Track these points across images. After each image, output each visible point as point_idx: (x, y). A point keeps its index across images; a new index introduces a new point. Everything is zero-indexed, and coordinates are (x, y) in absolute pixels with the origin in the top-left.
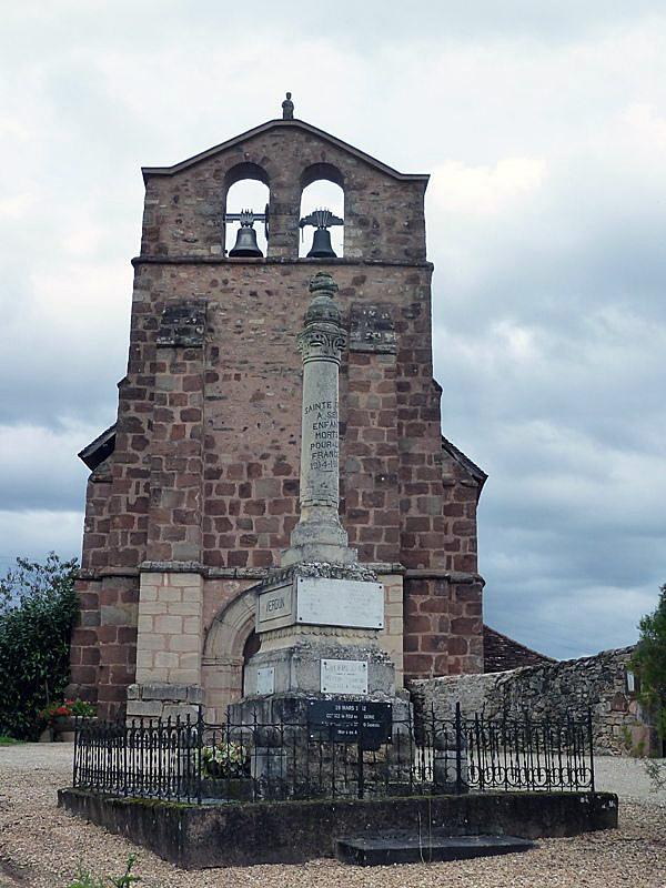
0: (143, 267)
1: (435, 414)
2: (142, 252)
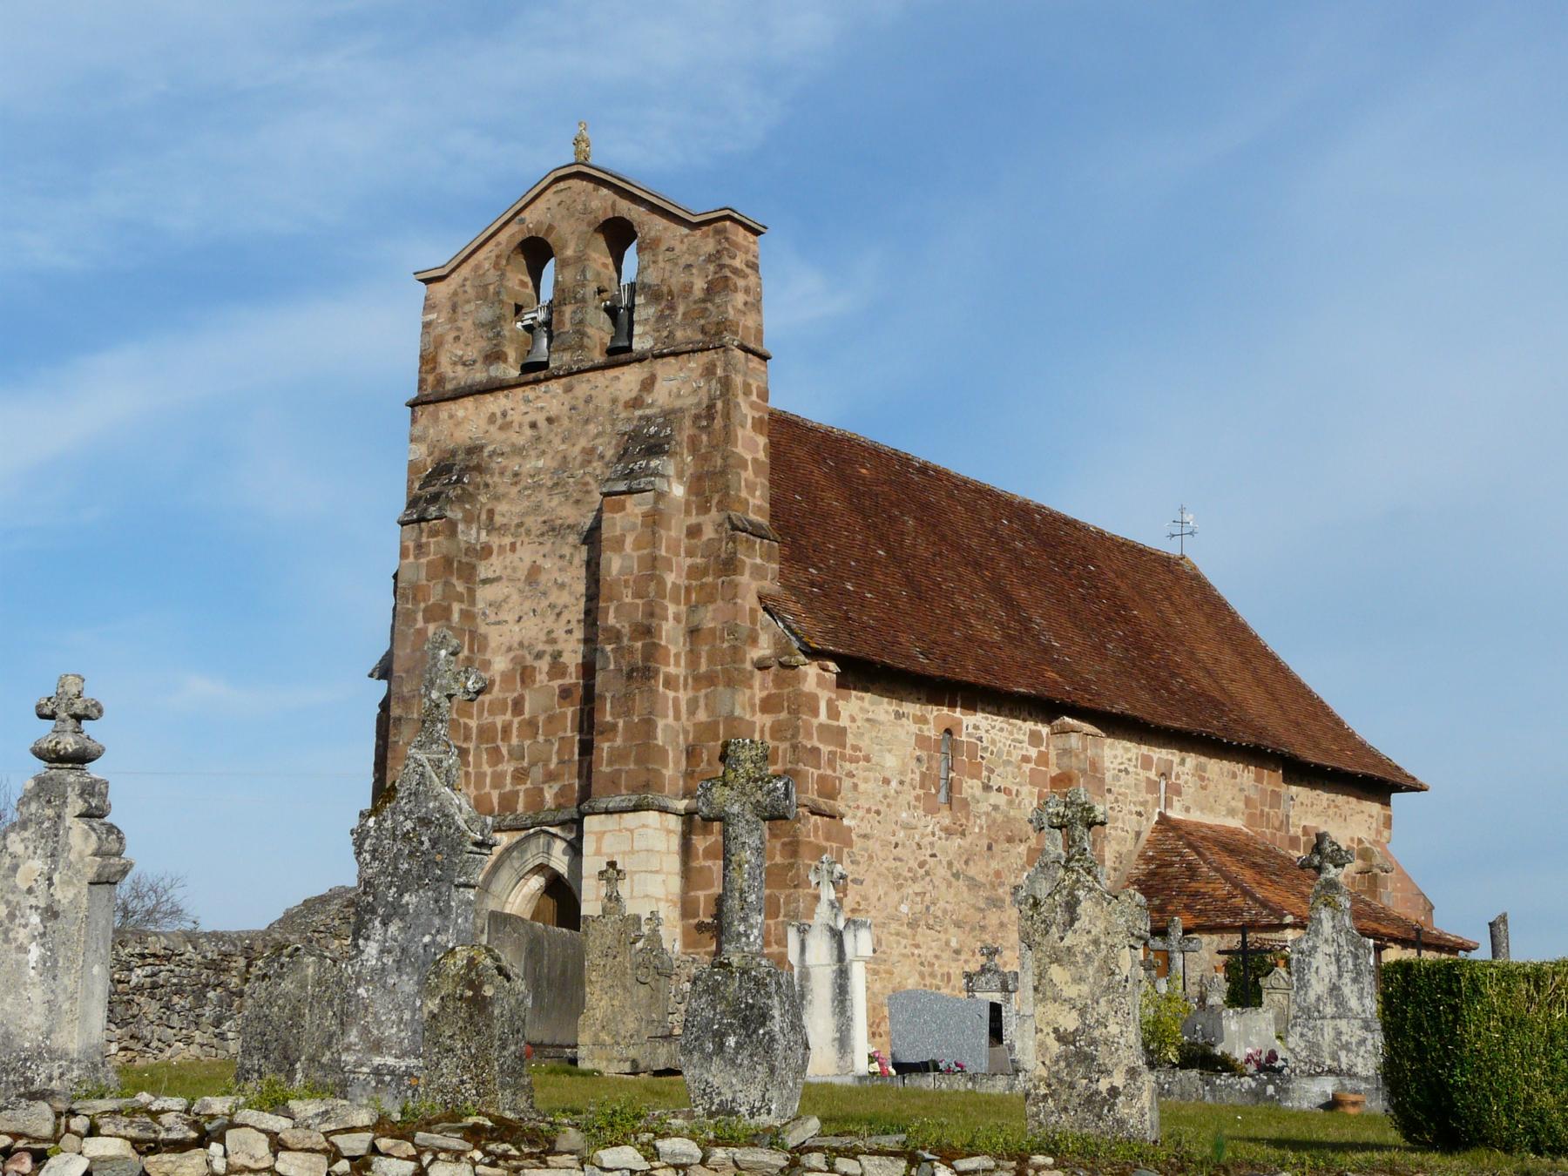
2: (420, 388)
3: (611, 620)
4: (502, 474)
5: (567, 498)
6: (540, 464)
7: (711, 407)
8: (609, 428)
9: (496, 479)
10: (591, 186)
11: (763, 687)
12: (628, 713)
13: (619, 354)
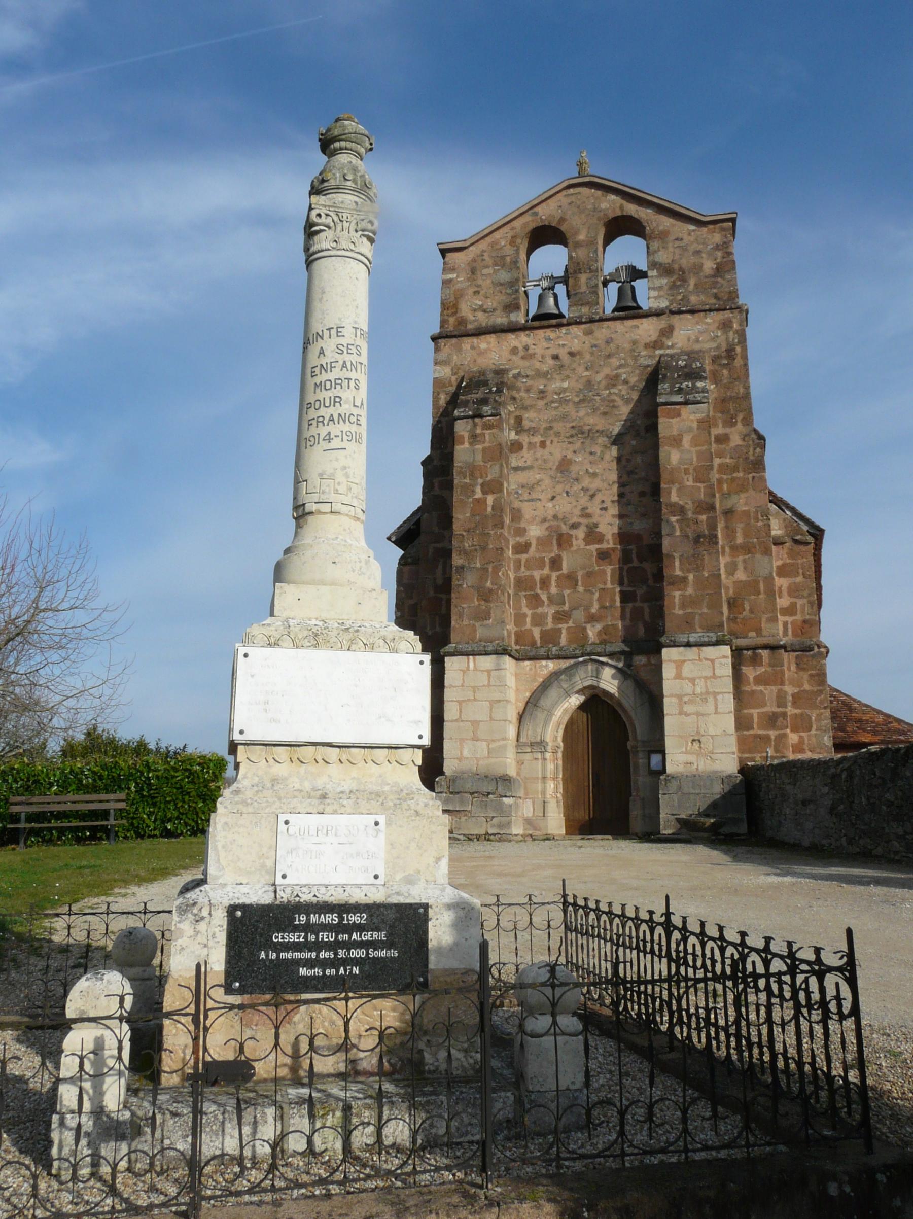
0: (442, 342)
1: (758, 465)
3: (674, 498)
4: (528, 390)
5: (595, 410)
6: (566, 385)
12: (698, 569)
13: (628, 309)
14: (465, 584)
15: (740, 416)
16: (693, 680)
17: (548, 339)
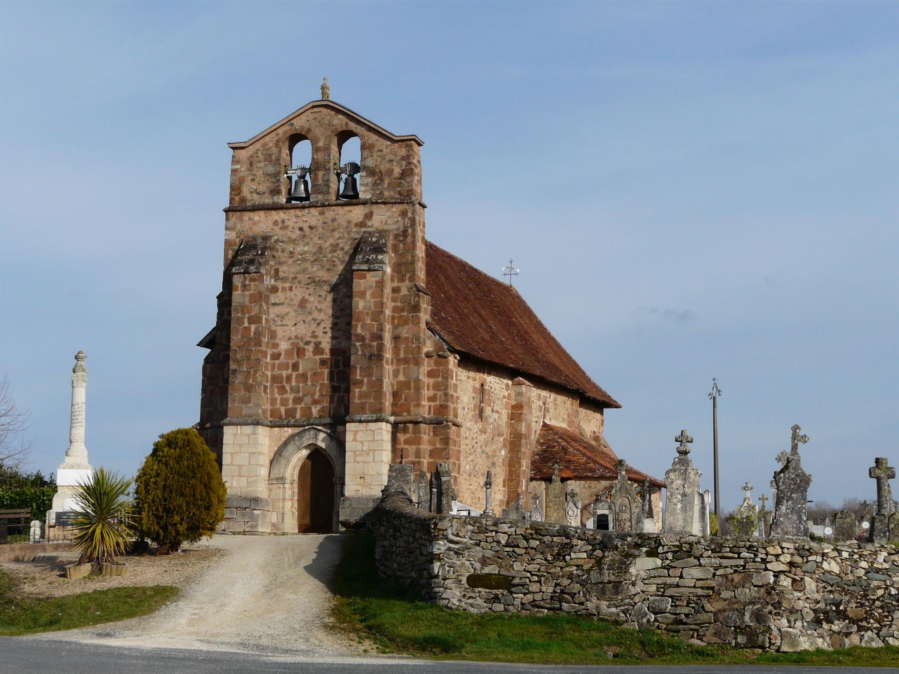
0: (230, 214)
2: (231, 203)
3: (359, 331)
4: (283, 251)
5: (322, 267)
6: (306, 249)
7: (405, 231)
8: (346, 235)
9: (279, 254)
10: (333, 113)
11: (428, 365)
12: (370, 375)
13: (351, 197)
14: (237, 380)
15: (408, 275)
16: (362, 443)
17: (297, 216)
